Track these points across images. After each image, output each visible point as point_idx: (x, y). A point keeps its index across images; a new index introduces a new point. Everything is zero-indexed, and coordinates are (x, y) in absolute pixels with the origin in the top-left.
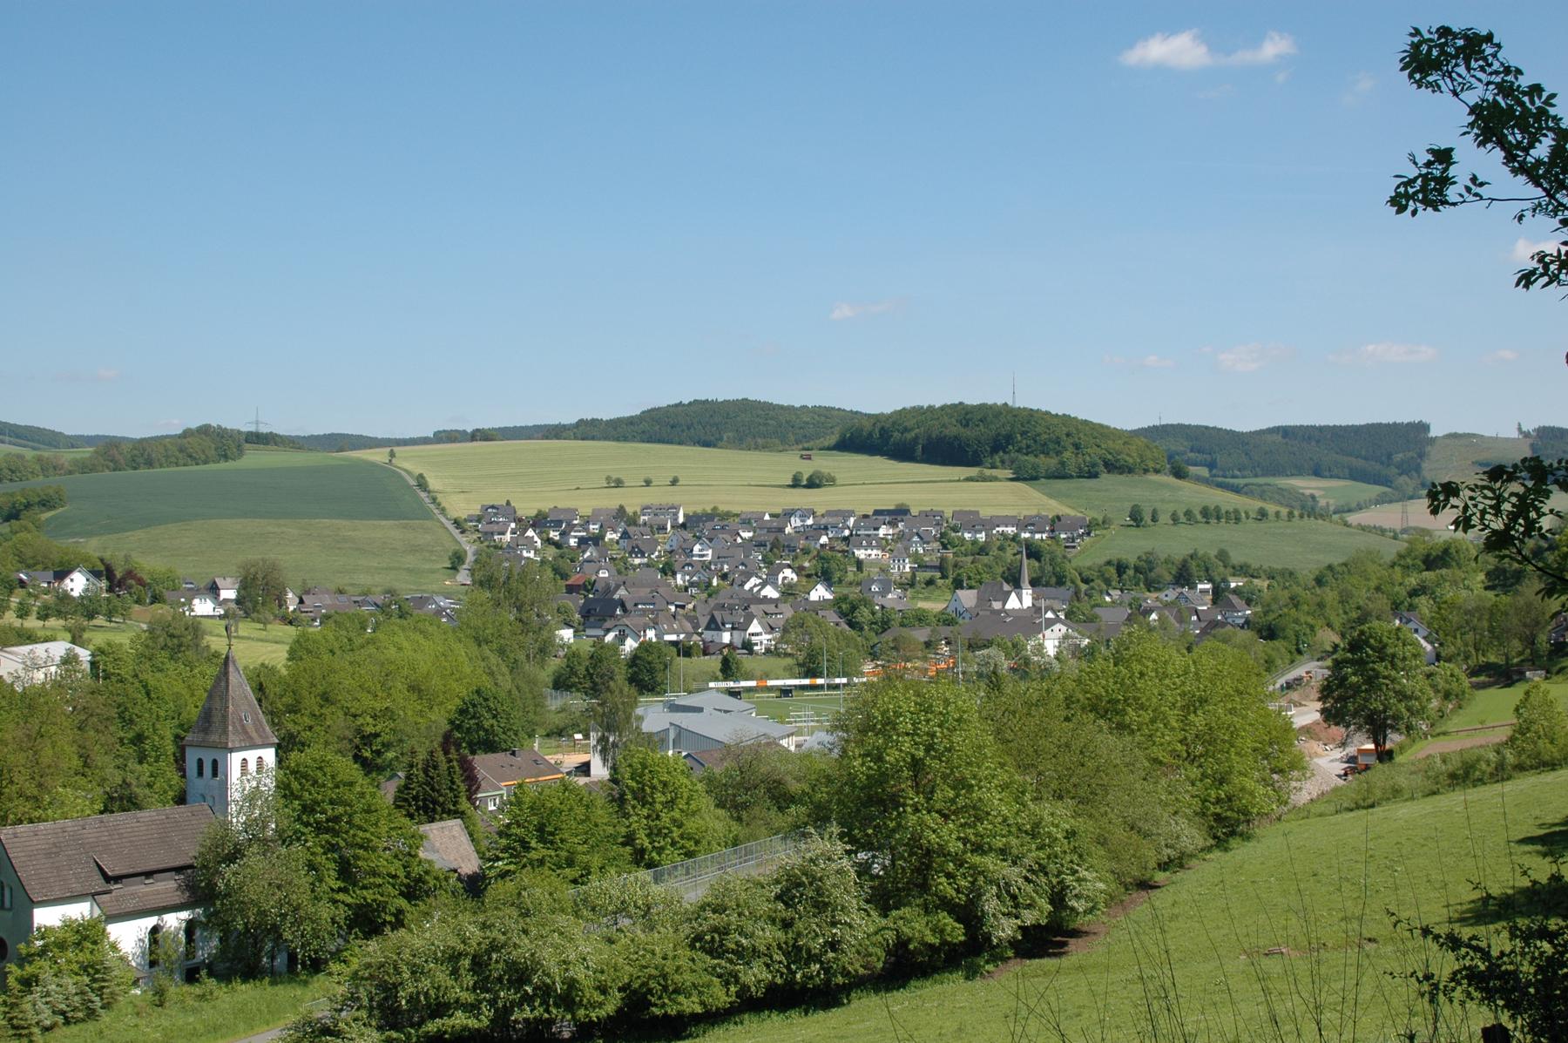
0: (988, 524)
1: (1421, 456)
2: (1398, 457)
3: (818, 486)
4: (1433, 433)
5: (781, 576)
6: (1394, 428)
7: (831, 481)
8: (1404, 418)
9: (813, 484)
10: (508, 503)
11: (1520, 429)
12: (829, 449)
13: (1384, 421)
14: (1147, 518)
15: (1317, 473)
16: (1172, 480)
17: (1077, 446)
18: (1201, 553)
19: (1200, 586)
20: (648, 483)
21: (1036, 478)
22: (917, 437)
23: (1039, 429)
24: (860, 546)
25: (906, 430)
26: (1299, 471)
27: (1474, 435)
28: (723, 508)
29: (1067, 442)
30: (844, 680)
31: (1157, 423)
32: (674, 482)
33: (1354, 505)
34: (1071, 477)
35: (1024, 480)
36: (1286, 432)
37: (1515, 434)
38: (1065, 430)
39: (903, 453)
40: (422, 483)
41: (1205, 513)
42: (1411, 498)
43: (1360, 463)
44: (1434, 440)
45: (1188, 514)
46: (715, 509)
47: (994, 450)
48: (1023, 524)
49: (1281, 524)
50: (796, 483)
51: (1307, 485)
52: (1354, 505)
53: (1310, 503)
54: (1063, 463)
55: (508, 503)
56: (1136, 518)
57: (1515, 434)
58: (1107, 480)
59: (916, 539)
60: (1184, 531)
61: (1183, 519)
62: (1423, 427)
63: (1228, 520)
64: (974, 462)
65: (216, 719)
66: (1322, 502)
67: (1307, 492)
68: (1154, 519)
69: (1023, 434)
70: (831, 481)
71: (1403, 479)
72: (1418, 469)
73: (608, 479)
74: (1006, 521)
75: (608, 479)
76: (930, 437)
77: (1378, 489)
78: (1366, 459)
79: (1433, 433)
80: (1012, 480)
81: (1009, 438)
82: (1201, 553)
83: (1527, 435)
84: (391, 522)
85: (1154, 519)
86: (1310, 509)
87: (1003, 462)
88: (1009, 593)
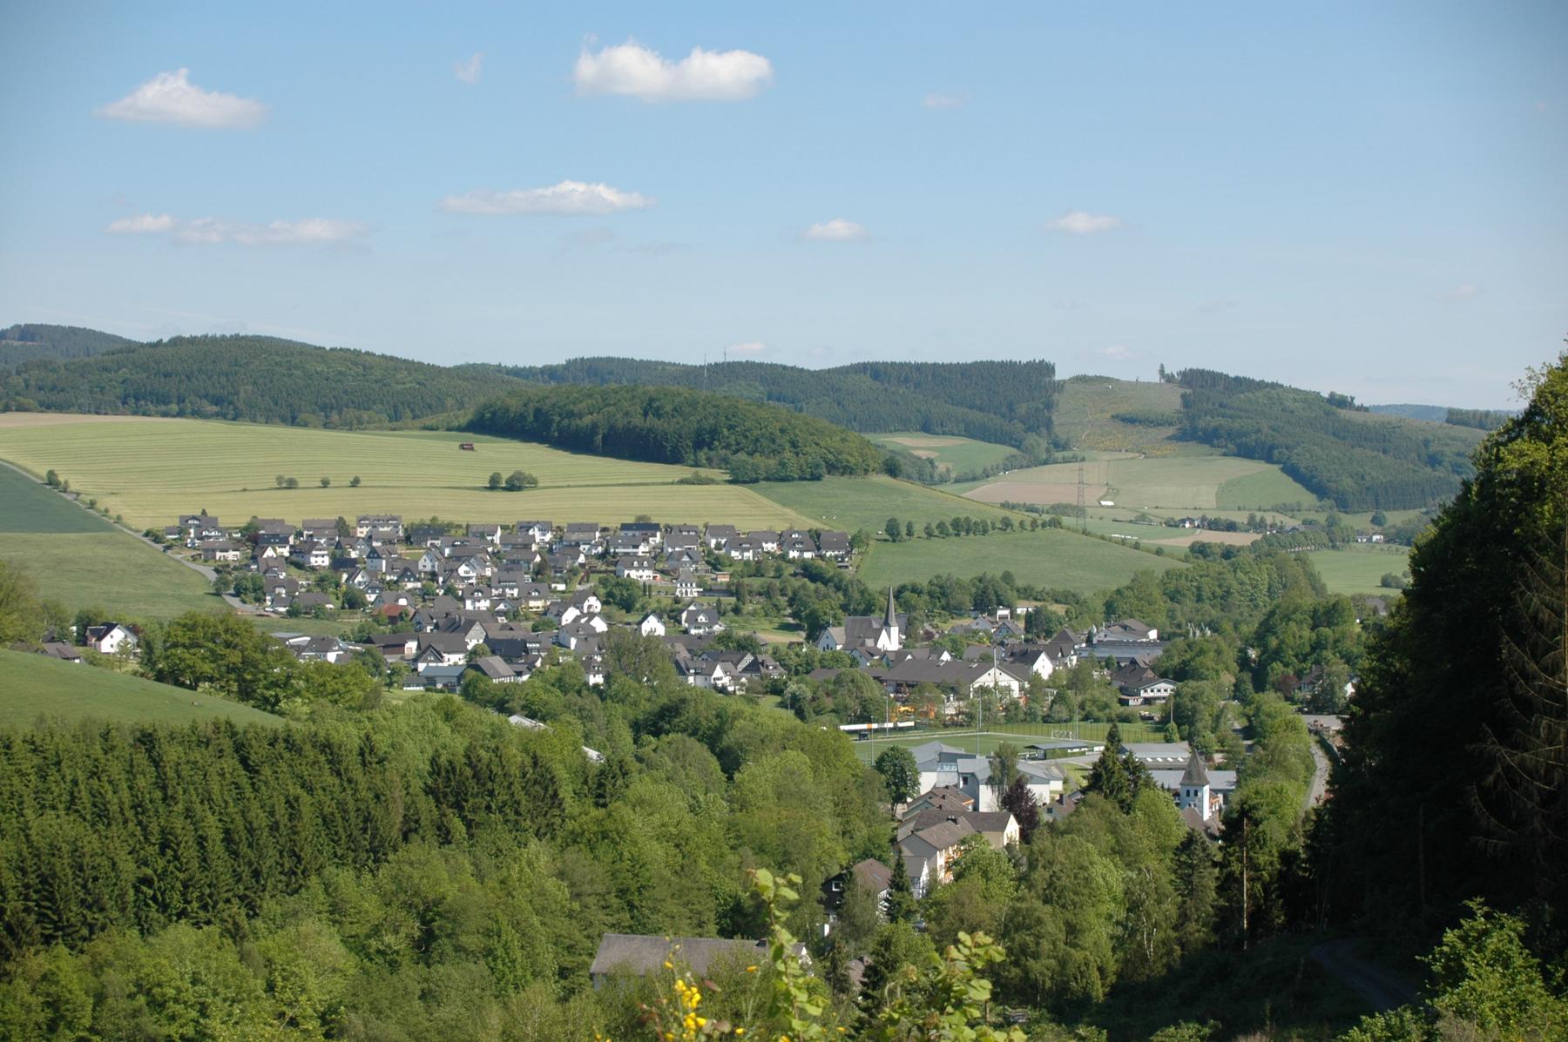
0: (754, 541)
1: (1049, 406)
2: (1022, 409)
3: (519, 489)
4: (1060, 375)
5: (586, 605)
6: (1009, 368)
7: (533, 483)
8: (1023, 357)
9: (514, 485)
10: (204, 512)
11: (1162, 371)
12: (460, 429)
13: (997, 359)
14: (903, 531)
15: (926, 428)
16: (885, 479)
17: (794, 445)
18: (989, 576)
19: (1000, 613)
20: (325, 484)
21: (756, 481)
22: (595, 426)
23: (748, 424)
24: (631, 567)
25: (571, 414)
26: (905, 426)
27: (1107, 380)
28: (444, 518)
29: (784, 441)
30: (891, 725)
31: (721, 360)
32: (355, 483)
33: (979, 471)
34: (793, 479)
35: (744, 482)
36: (876, 371)
37: (1155, 378)
38: (778, 425)
39: (576, 442)
40: (52, 480)
41: (956, 524)
42: (1045, 463)
43: (976, 416)
44: (1061, 386)
45: (941, 526)
46: (434, 519)
47: (699, 445)
48: (781, 539)
49: (1026, 534)
50: (494, 485)
51: (918, 445)
52: (979, 471)
53: (928, 470)
54: (783, 464)
55: (204, 512)
56: (893, 532)
57: (1155, 378)
58: (831, 482)
59: (686, 558)
60: (937, 544)
61: (936, 532)
62: (1045, 369)
63: (941, 526)
64: (674, 458)
65: (1195, 774)
66: (941, 467)
67: (923, 454)
68: (910, 534)
69: (730, 428)
70: (533, 483)
71: (1031, 439)
72: (1049, 424)
73: (280, 479)
74: (769, 536)
75: (280, 479)
76: (612, 428)
77: (1003, 451)
78: (981, 409)
79: (1060, 375)
80: (730, 482)
81: (714, 433)
82: (989, 576)
83: (1169, 379)
84: (73, 536)
85: (910, 534)
86: (925, 474)
87: (709, 460)
88: (880, 631)
